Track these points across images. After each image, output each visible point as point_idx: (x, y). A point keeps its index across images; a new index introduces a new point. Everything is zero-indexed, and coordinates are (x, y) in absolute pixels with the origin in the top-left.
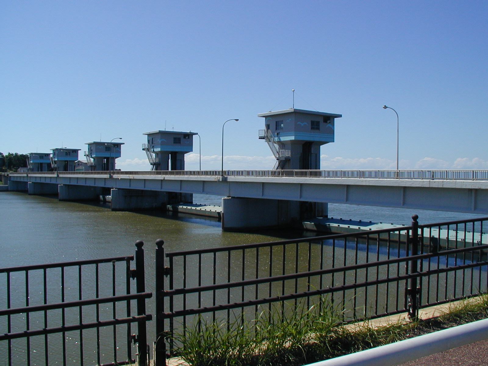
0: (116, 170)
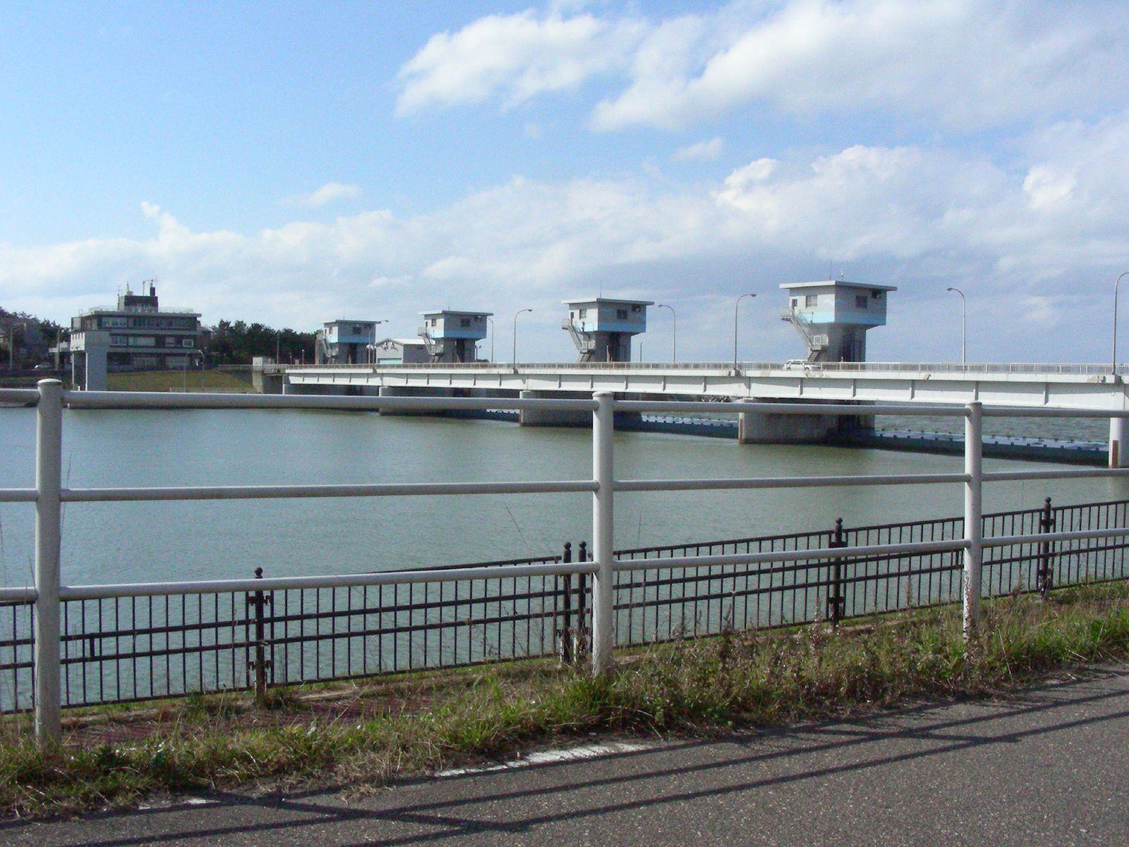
0: (478, 361)
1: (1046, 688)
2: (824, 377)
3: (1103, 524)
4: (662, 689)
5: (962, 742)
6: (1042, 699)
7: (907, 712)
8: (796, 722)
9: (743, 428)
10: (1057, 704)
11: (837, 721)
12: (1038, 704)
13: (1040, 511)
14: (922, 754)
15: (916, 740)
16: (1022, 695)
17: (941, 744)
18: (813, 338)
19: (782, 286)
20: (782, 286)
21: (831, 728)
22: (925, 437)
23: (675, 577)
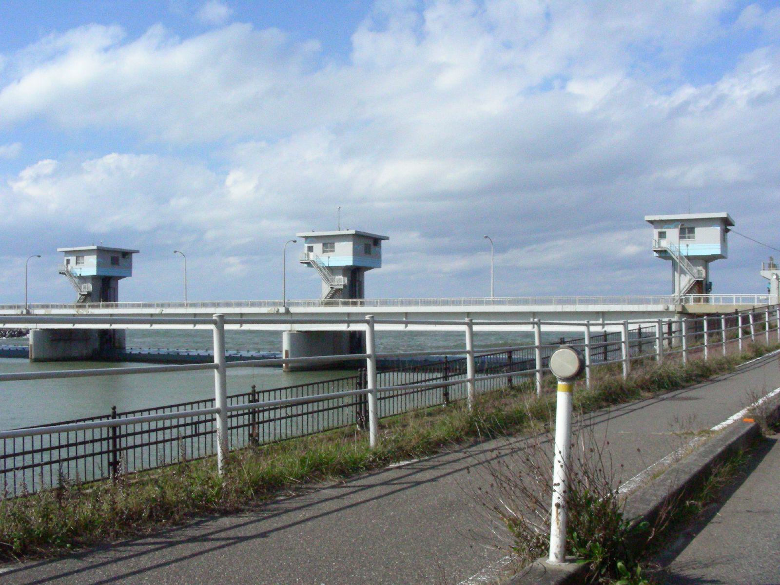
1: (277, 502)
2: (90, 313)
3: (387, 384)
4: (17, 525)
5: (231, 541)
6: (275, 509)
7: (190, 526)
8: (115, 541)
9: (33, 350)
10: (287, 511)
11: (143, 537)
12: (275, 512)
13: (249, 394)
14: (207, 551)
15: (200, 543)
16: (263, 508)
17: (218, 544)
18: (81, 287)
19: (59, 250)
20: (59, 250)
21: (139, 541)
22: (161, 353)
23: (187, 422)
